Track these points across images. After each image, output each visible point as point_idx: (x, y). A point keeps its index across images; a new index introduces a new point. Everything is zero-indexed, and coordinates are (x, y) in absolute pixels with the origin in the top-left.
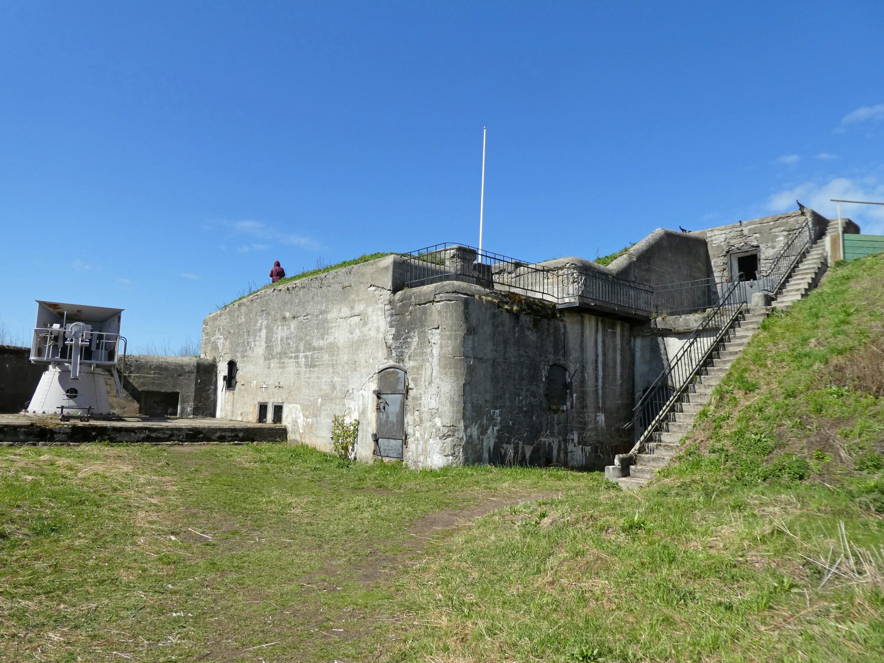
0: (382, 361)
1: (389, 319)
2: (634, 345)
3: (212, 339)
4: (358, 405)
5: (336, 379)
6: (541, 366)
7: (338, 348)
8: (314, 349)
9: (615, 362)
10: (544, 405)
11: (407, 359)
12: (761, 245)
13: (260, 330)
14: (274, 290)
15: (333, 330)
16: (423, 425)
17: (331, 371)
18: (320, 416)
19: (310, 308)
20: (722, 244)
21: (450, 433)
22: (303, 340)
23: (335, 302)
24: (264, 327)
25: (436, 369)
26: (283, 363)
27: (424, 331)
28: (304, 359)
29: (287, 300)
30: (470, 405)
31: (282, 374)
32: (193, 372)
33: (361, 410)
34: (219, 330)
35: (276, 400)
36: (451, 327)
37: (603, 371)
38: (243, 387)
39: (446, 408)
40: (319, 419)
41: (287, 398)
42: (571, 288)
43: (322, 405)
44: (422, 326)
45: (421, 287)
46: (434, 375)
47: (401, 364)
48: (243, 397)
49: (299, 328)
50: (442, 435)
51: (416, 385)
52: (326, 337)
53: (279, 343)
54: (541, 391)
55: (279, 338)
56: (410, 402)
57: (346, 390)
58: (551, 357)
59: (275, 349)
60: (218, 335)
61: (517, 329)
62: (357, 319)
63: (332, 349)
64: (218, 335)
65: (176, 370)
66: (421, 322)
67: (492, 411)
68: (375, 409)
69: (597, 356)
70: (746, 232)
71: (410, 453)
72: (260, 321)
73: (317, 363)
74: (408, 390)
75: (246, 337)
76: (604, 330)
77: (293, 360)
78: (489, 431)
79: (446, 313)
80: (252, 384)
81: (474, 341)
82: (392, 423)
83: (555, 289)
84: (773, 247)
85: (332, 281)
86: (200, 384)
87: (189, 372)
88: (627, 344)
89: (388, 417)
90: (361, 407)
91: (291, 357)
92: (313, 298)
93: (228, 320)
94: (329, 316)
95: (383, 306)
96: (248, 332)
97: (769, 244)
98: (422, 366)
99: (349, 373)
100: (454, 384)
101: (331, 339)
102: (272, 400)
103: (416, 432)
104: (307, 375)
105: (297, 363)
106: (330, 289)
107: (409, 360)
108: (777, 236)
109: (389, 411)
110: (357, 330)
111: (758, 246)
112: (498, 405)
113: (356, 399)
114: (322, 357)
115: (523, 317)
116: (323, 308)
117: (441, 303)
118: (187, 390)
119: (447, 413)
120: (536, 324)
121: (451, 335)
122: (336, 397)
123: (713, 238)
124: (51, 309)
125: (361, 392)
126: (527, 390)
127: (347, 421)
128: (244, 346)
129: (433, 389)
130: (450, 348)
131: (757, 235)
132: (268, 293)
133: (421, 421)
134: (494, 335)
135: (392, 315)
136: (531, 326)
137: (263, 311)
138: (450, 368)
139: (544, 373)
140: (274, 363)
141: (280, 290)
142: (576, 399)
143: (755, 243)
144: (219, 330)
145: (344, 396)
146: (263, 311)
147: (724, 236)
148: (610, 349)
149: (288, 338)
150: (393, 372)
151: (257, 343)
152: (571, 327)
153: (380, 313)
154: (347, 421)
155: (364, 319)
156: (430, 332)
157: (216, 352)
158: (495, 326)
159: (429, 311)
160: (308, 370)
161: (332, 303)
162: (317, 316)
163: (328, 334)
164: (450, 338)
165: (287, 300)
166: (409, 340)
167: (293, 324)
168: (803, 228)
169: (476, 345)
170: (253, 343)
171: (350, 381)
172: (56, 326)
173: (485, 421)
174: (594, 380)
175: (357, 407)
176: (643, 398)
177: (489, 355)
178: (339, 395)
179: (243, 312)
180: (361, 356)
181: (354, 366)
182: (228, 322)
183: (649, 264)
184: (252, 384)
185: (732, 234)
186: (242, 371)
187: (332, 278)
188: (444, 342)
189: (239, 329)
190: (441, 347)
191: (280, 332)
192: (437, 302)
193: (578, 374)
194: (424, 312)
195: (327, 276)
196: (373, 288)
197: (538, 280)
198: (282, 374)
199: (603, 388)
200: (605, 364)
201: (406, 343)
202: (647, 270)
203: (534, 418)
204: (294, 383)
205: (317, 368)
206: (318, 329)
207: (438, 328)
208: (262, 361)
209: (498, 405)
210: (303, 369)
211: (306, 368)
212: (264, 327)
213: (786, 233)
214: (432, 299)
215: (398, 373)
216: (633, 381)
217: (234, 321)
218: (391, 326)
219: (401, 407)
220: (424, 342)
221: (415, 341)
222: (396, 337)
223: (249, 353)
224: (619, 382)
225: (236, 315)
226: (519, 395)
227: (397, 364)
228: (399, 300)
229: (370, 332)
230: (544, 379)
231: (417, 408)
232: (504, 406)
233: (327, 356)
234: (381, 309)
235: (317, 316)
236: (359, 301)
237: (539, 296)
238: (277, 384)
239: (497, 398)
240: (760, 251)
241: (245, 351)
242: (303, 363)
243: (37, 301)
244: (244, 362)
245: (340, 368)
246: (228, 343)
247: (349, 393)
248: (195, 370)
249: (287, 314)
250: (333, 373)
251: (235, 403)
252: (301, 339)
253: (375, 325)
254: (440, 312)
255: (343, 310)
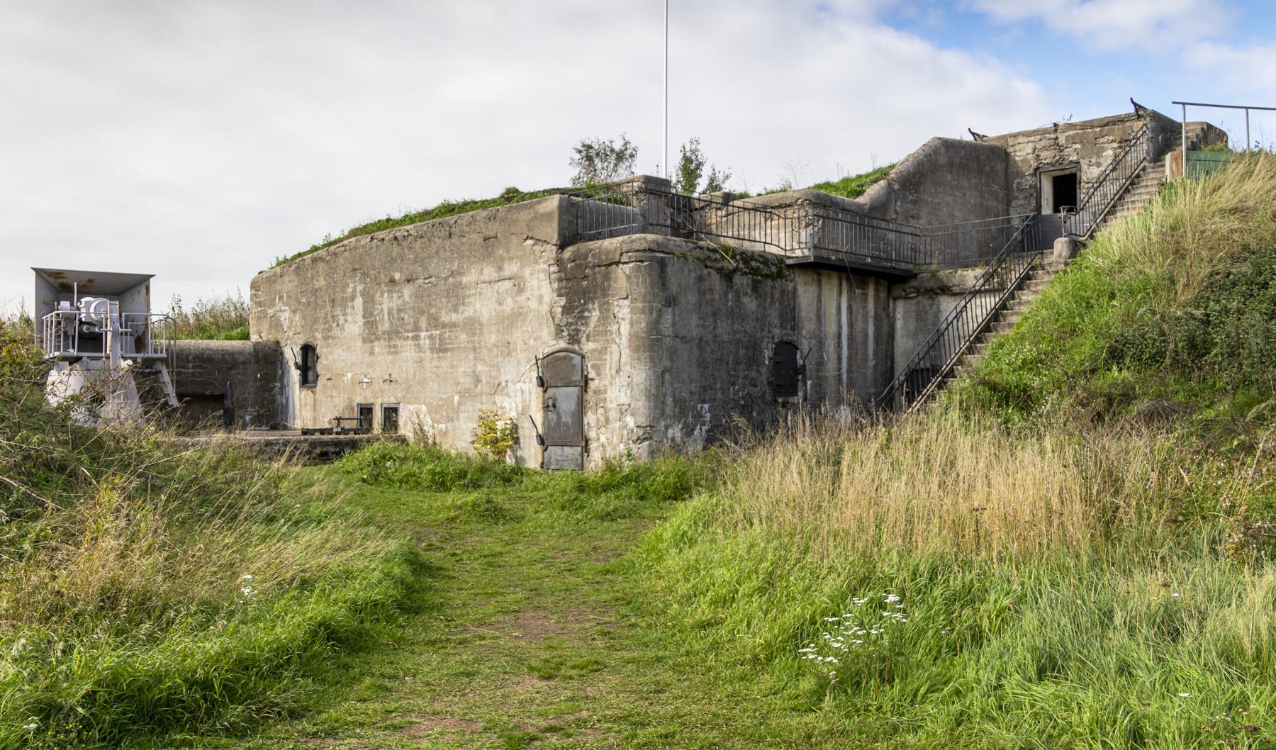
0: (549, 342)
1: (556, 285)
2: (894, 310)
3: (270, 312)
4: (516, 403)
5: (480, 368)
6: (764, 345)
7: (481, 325)
8: (444, 326)
9: (866, 336)
10: (768, 398)
11: (584, 339)
12: (1081, 161)
13: (353, 298)
14: (372, 238)
15: (472, 299)
16: (610, 426)
17: (471, 356)
18: (458, 420)
19: (433, 267)
20: (1029, 157)
21: (646, 435)
22: (424, 312)
23: (472, 260)
24: (358, 294)
25: (626, 352)
26: (395, 346)
27: (607, 303)
28: (427, 341)
29: (394, 254)
30: (671, 399)
31: (393, 362)
32: (250, 363)
33: (520, 409)
34: (281, 298)
35: (386, 400)
36: (644, 296)
37: (849, 348)
38: (329, 383)
39: (640, 403)
40: (457, 423)
41: (404, 397)
42: (803, 233)
43: (460, 404)
44: (605, 295)
45: (600, 242)
46: (622, 360)
47: (576, 347)
48: (332, 397)
49: (418, 296)
50: (635, 438)
51: (598, 374)
52: (461, 308)
53: (386, 317)
54: (764, 378)
55: (386, 311)
56: (590, 396)
57: (497, 382)
58: (777, 331)
59: (380, 326)
60: (279, 306)
61: (730, 296)
62: (508, 284)
63: (473, 326)
64: (279, 306)
65: (224, 360)
66: (603, 290)
67: (699, 406)
68: (541, 406)
69: (840, 327)
70: (1062, 140)
71: (593, 464)
72: (351, 286)
73: (450, 346)
74: (586, 380)
75: (328, 308)
76: (851, 290)
77: (410, 342)
78: (695, 433)
79: (637, 277)
80: (345, 378)
81: (674, 314)
82: (566, 425)
83: (782, 235)
84: (1099, 165)
85: (467, 229)
86: (260, 380)
87: (243, 363)
88: (884, 309)
89: (559, 417)
90: (520, 406)
91: (408, 338)
92: (437, 252)
93: (296, 283)
94: (465, 280)
95: (546, 266)
96: (333, 301)
97: (1094, 161)
98: (606, 348)
99: (500, 359)
100: (650, 372)
101: (469, 312)
102: (379, 401)
103: (601, 436)
104: (435, 363)
105: (418, 346)
106: (464, 240)
107: (588, 340)
108: (1103, 149)
109: (561, 411)
110: (509, 300)
111: (1078, 163)
112: (707, 397)
113: (512, 394)
114: (457, 338)
115: (738, 279)
116: (455, 267)
117: (631, 265)
118: (245, 389)
119: (642, 410)
120: (755, 286)
121: (644, 307)
122: (481, 394)
123: (1017, 148)
124: (51, 280)
125: (519, 385)
126: (746, 377)
127: (500, 425)
128: (328, 322)
129: (623, 379)
130: (643, 325)
131: (1078, 146)
132: (363, 243)
133: (607, 421)
134: (700, 306)
135: (560, 280)
136: (749, 291)
137: (355, 270)
138: (644, 351)
139: (767, 354)
140: (378, 347)
141: (383, 240)
142: (811, 388)
143: (1074, 158)
144: (281, 298)
145: (493, 391)
146: (355, 270)
147: (1031, 145)
148: (860, 317)
149: (399, 311)
150: (565, 357)
151: (349, 318)
152: (805, 292)
153: (542, 276)
154: (500, 425)
155: (519, 284)
156: (615, 303)
157: (277, 331)
158: (701, 293)
159: (613, 276)
160: (435, 355)
161: (469, 261)
162: (446, 279)
163: (464, 304)
164: (643, 312)
165: (394, 254)
166: (586, 314)
167: (407, 291)
168: (1138, 139)
169: (677, 319)
170: (342, 318)
171: (502, 371)
172: (65, 305)
173: (690, 420)
174: (836, 362)
175: (514, 405)
176: (214, 344)
177: (695, 333)
178: (486, 389)
179: (321, 270)
180: (517, 336)
181: (507, 349)
182: (297, 286)
183: (917, 192)
184: (345, 378)
185: (1043, 143)
186: (326, 359)
187: (467, 225)
188: (635, 317)
189: (317, 297)
190: (632, 324)
191: (386, 302)
192: (623, 263)
193: (814, 354)
194: (607, 277)
195: (459, 222)
196: (530, 242)
197: (758, 221)
198: (393, 362)
199: (849, 371)
200: (851, 339)
201: (582, 319)
202: (915, 202)
203: (754, 414)
204: (415, 374)
205: (449, 354)
206: (448, 297)
207: (627, 298)
208: (359, 343)
209: (707, 397)
210: (428, 353)
211: (432, 352)
212: (358, 294)
213: (1115, 145)
214: (617, 259)
215: (572, 359)
216: (893, 361)
217: (307, 284)
218: (560, 295)
219: (578, 404)
220: (607, 316)
221: (595, 315)
222: (567, 310)
223: (336, 332)
224: (872, 363)
225: (309, 275)
226: (734, 384)
227: (571, 346)
228: (569, 259)
229: (529, 303)
230: (767, 362)
231: (601, 402)
232: (715, 400)
233: (464, 336)
234: (543, 271)
235: (446, 279)
236: (511, 259)
237: (759, 247)
238: (387, 377)
239: (705, 388)
240: (1080, 170)
241: (330, 329)
242: (427, 346)
243: (33, 269)
244: (328, 346)
245: (485, 352)
246: (297, 317)
247: (501, 388)
248: (253, 361)
249: (397, 276)
250: (475, 359)
251: (318, 408)
252: (422, 312)
253: (536, 293)
254: (628, 277)
255: (485, 271)
